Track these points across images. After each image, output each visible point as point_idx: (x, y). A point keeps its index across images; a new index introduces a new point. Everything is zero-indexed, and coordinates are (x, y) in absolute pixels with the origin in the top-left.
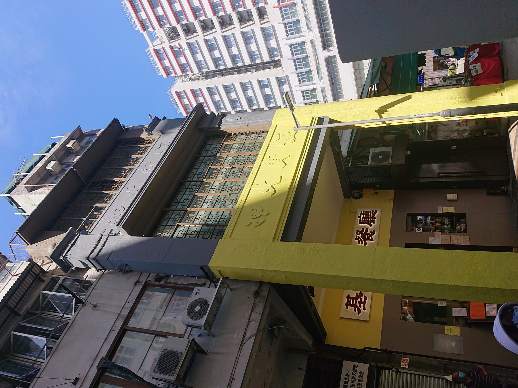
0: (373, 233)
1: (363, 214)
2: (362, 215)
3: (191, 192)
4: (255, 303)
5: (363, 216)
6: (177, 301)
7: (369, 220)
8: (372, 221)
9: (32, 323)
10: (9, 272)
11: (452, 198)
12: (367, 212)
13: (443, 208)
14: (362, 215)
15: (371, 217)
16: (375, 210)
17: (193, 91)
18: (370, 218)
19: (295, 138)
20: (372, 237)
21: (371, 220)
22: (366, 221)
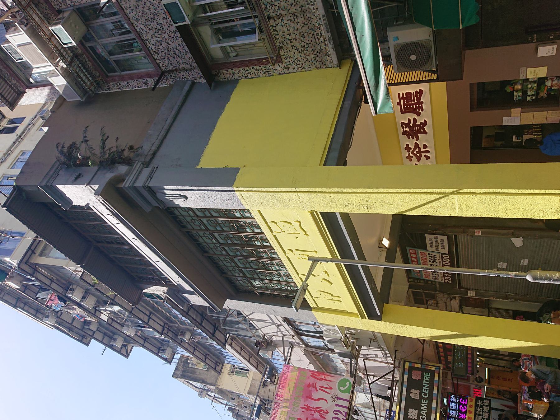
0: (425, 123)
1: (403, 98)
2: (402, 101)
3: (214, 248)
4: (187, 15)
5: (404, 102)
6: (399, 266)
7: (414, 106)
8: (419, 108)
9: (548, 269)
10: (51, 288)
11: (547, 55)
12: (410, 100)
13: (528, 69)
14: (402, 101)
15: (416, 102)
16: (420, 90)
17: (451, 259)
18: (416, 104)
19: (306, 232)
20: (424, 130)
21: (420, 105)
22: (410, 108)
